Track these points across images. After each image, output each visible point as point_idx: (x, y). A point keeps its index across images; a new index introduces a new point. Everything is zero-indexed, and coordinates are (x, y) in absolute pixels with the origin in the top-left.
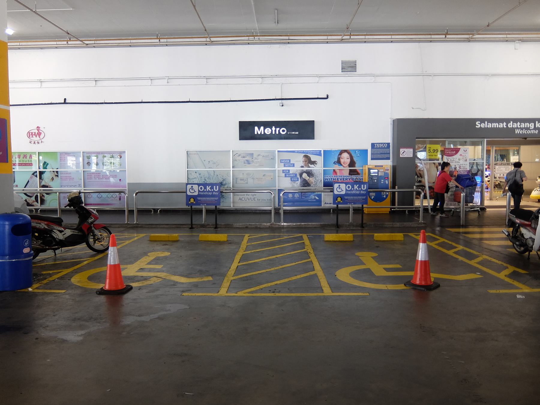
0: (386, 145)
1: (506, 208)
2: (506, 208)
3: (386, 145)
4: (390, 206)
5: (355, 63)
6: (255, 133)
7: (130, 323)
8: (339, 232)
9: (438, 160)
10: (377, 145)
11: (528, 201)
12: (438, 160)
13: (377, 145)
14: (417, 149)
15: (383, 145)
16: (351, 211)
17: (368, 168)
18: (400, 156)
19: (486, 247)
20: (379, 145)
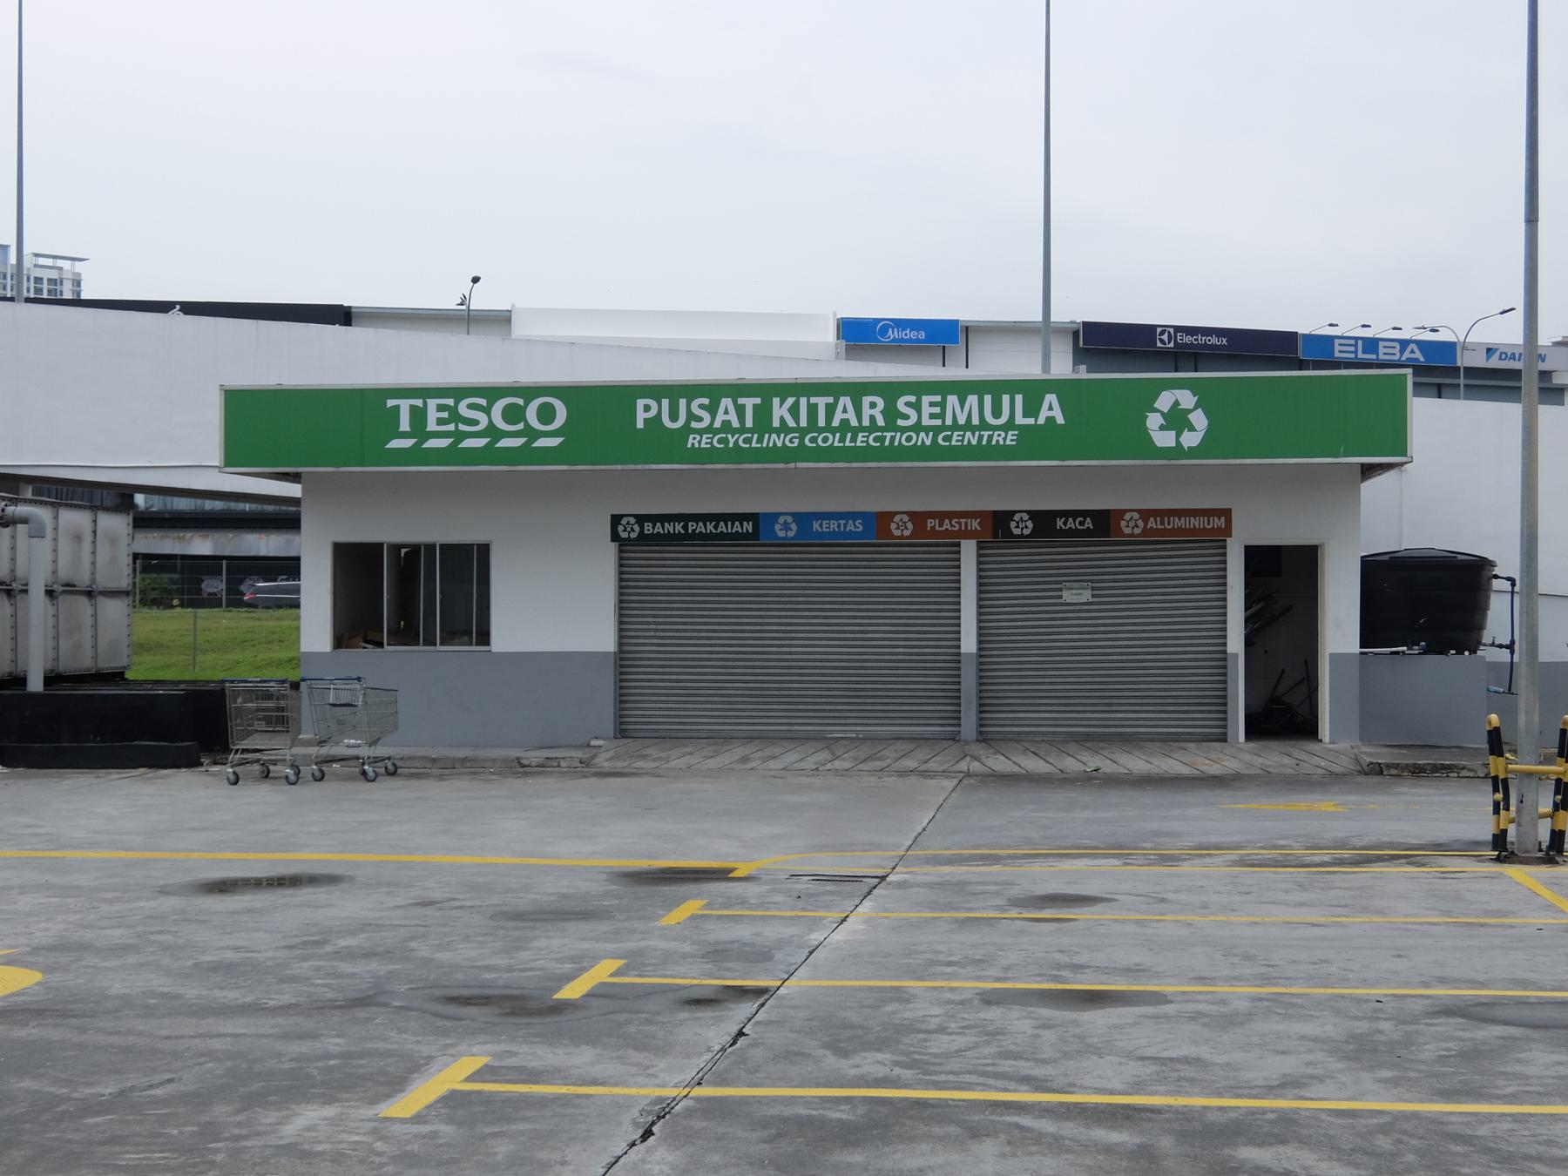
0: (546, 414)
1: (1330, 743)
2: (1330, 743)
3: (546, 414)
4: (1460, 378)
5: (930, 406)
6: (398, 425)
7: (63, 783)
8: (1444, 392)
9: (438, 405)
10: (418, 415)
11: (1406, 550)
12: (438, 405)
13: (418, 415)
14: (735, 402)
15: (513, 414)
16: (4, 281)
17: (1406, 374)
18: (638, 401)
19: (1479, 361)
20: (455, 417)
